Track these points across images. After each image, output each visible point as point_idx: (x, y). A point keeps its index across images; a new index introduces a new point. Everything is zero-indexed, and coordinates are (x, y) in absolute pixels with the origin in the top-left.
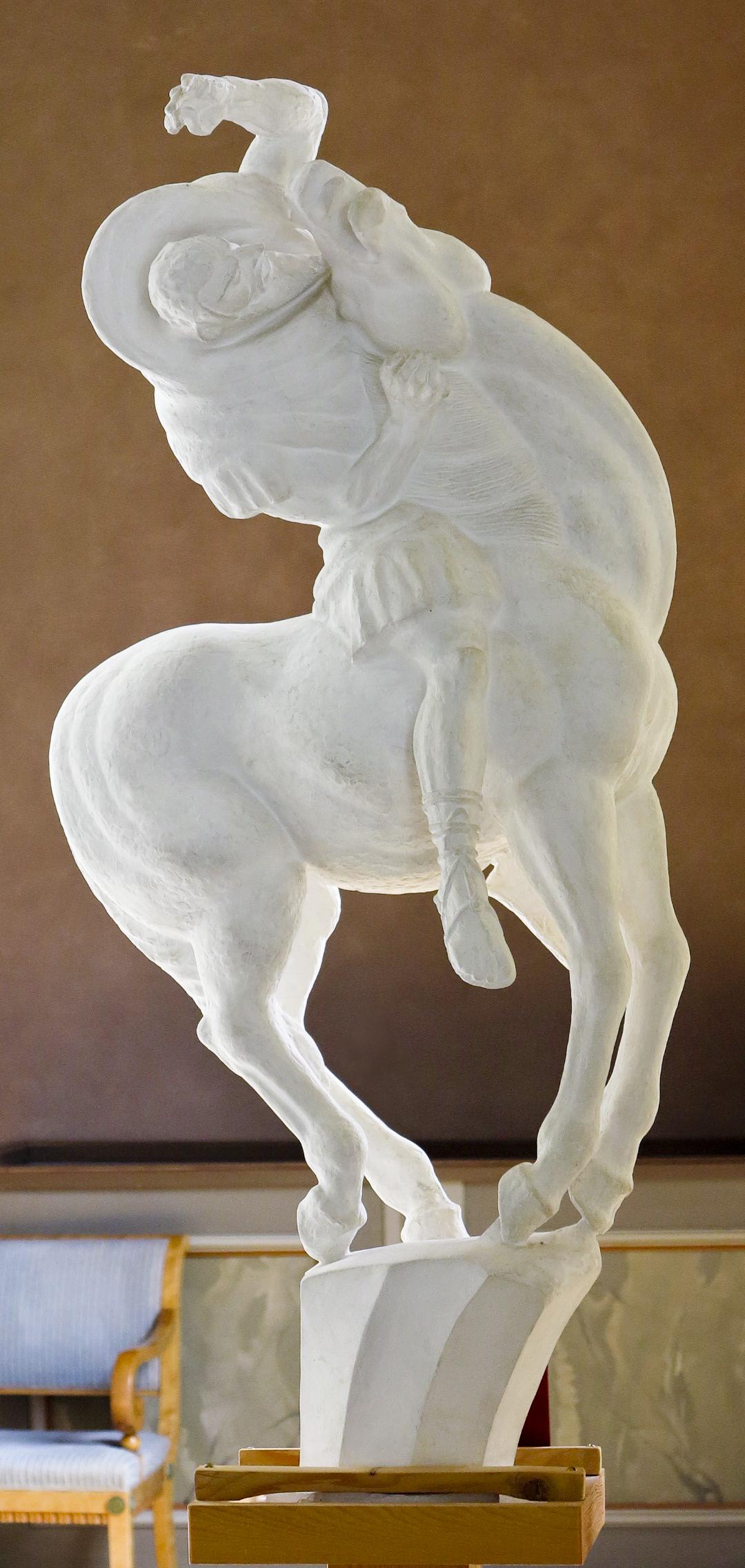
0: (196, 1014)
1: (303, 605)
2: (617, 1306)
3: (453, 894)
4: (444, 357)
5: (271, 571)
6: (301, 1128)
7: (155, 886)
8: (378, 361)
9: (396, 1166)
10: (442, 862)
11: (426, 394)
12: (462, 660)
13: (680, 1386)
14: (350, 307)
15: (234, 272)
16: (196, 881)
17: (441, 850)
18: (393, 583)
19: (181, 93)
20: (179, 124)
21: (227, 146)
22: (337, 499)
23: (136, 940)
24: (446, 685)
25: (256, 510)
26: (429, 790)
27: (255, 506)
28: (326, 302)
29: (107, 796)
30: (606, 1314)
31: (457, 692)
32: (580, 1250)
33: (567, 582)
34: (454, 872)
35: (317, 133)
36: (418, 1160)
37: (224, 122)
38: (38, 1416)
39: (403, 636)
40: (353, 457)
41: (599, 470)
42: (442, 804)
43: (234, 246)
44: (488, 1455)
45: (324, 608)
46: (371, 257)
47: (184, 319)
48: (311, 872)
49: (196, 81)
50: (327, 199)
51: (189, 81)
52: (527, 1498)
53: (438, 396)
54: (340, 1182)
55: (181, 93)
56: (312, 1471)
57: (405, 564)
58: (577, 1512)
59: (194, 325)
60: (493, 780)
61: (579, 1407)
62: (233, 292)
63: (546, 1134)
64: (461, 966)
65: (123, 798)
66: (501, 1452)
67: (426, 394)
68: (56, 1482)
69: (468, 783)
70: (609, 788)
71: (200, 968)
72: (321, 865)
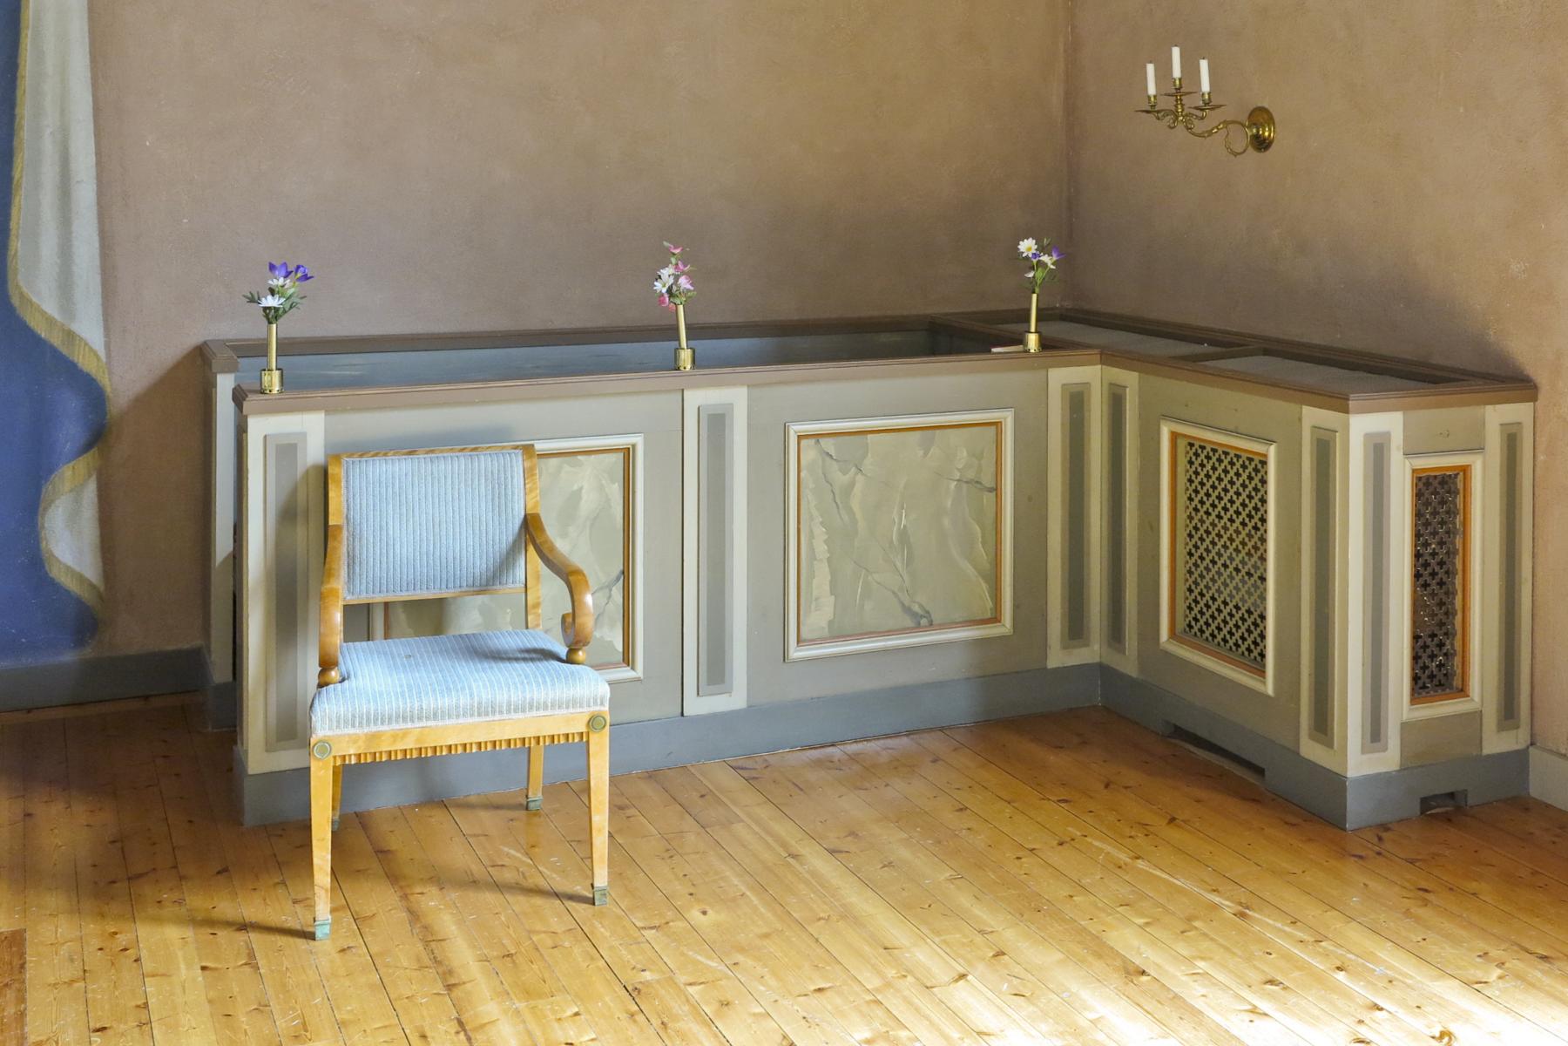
2: (859, 477)
13: (903, 534)
28: (118, 845)
30: (852, 484)
61: (829, 560)
68: (404, 719)
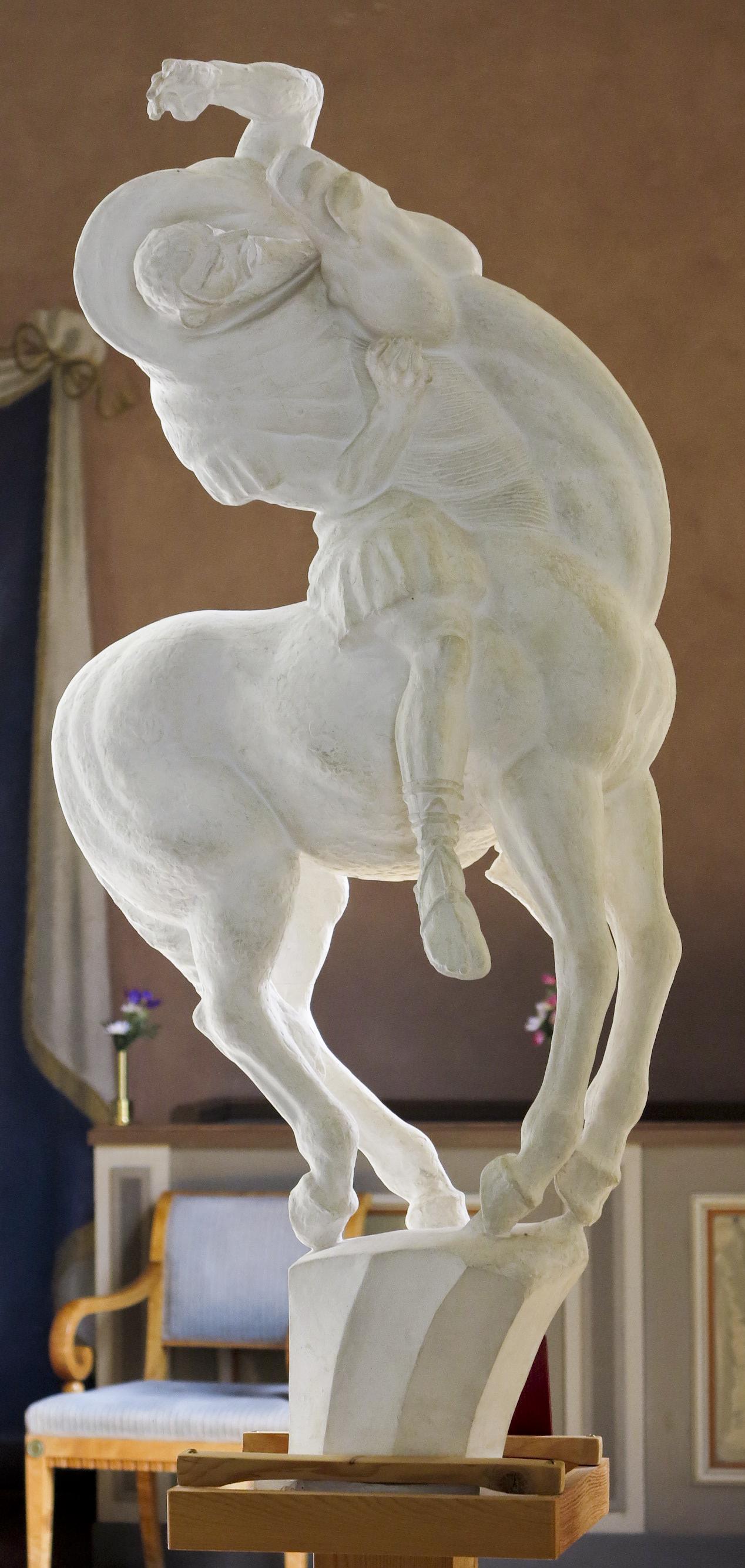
0: (193, 998)
1: (296, 591)
3: (428, 886)
4: (431, 341)
5: (266, 558)
6: (294, 1117)
7: (148, 873)
8: (364, 345)
9: (404, 1156)
10: (419, 851)
11: (409, 380)
12: (442, 648)
14: (338, 292)
15: (217, 258)
16: (187, 869)
17: (419, 839)
18: (377, 571)
19: (161, 79)
20: (159, 110)
21: (219, 131)
22: (328, 488)
23: (136, 925)
24: (426, 673)
25: (247, 498)
26: (408, 780)
27: (246, 494)
29: (103, 784)
31: (437, 680)
32: (563, 1243)
33: (552, 569)
34: (430, 862)
35: (311, 118)
36: (421, 1148)
37: (211, 108)
38: (225, 1369)
39: (384, 625)
40: (344, 443)
41: (588, 455)
42: (420, 794)
43: (219, 232)
44: (471, 1446)
45: (316, 594)
46: (352, 242)
47: (167, 305)
48: (304, 859)
49: (178, 66)
50: (306, 187)
51: (171, 66)
52: (502, 1491)
53: (421, 383)
54: (331, 1170)
55: (161, 79)
56: (309, 1459)
57: (389, 551)
58: (550, 1508)
59: (178, 312)
60: (477, 769)
62: (215, 279)
63: (529, 1125)
64: (434, 957)
65: (117, 784)
66: (488, 1441)
67: (409, 380)
69: (447, 772)
70: (597, 778)
71: (196, 958)
72: (313, 852)
